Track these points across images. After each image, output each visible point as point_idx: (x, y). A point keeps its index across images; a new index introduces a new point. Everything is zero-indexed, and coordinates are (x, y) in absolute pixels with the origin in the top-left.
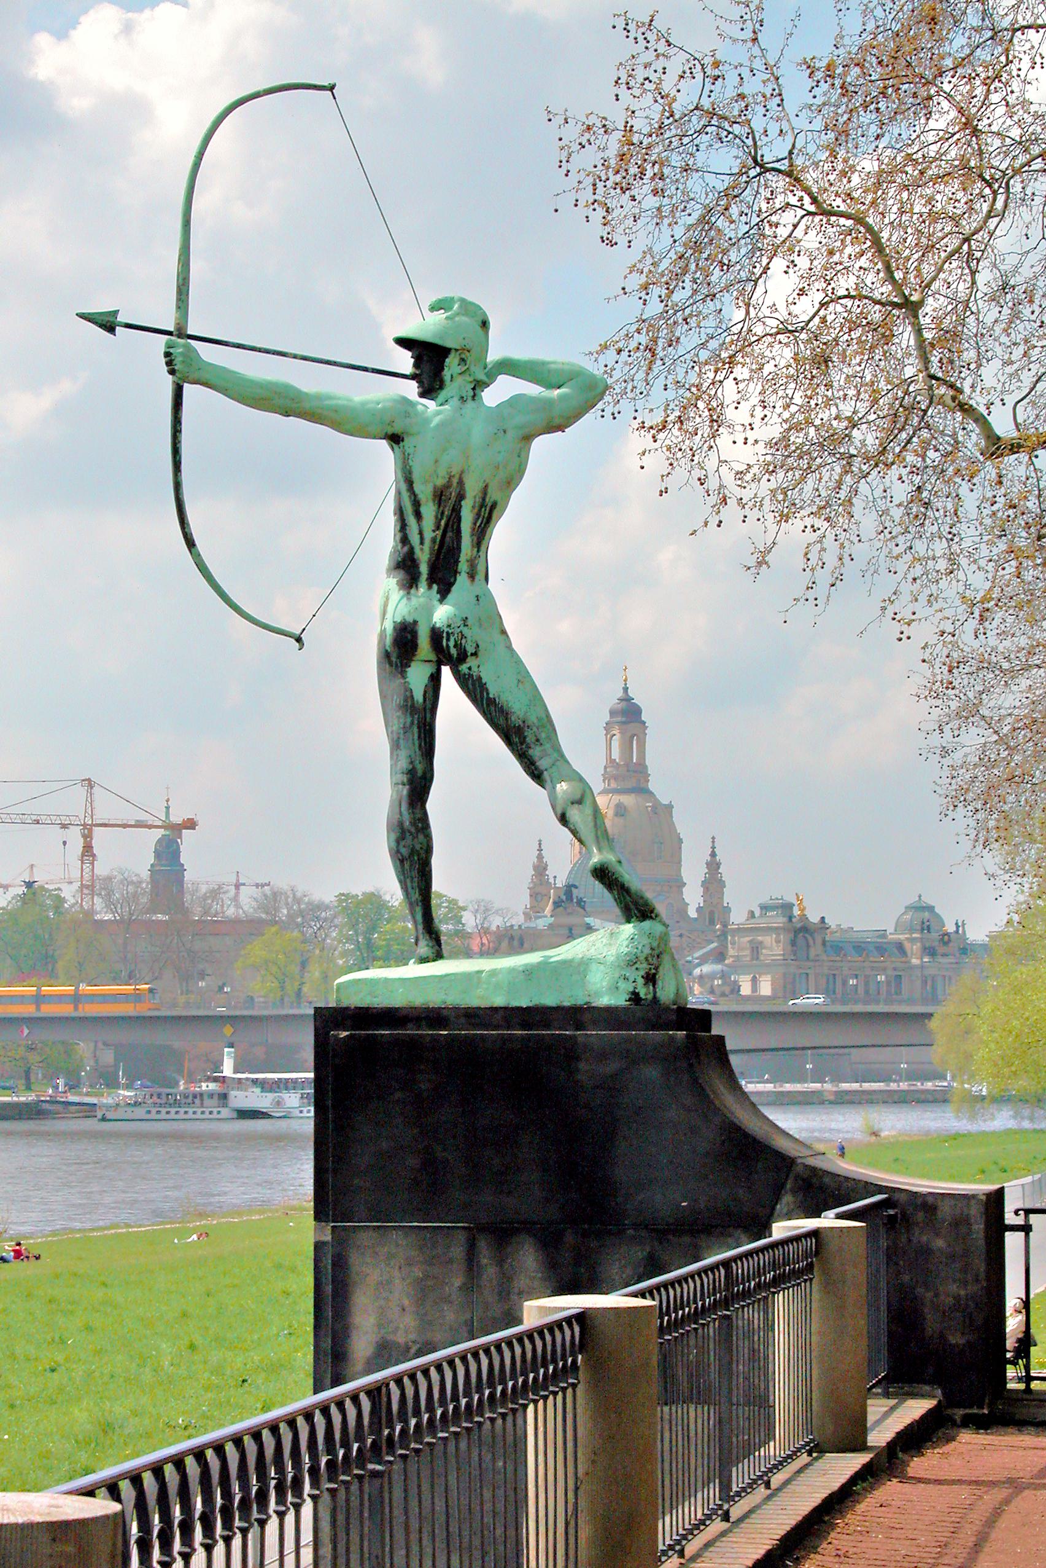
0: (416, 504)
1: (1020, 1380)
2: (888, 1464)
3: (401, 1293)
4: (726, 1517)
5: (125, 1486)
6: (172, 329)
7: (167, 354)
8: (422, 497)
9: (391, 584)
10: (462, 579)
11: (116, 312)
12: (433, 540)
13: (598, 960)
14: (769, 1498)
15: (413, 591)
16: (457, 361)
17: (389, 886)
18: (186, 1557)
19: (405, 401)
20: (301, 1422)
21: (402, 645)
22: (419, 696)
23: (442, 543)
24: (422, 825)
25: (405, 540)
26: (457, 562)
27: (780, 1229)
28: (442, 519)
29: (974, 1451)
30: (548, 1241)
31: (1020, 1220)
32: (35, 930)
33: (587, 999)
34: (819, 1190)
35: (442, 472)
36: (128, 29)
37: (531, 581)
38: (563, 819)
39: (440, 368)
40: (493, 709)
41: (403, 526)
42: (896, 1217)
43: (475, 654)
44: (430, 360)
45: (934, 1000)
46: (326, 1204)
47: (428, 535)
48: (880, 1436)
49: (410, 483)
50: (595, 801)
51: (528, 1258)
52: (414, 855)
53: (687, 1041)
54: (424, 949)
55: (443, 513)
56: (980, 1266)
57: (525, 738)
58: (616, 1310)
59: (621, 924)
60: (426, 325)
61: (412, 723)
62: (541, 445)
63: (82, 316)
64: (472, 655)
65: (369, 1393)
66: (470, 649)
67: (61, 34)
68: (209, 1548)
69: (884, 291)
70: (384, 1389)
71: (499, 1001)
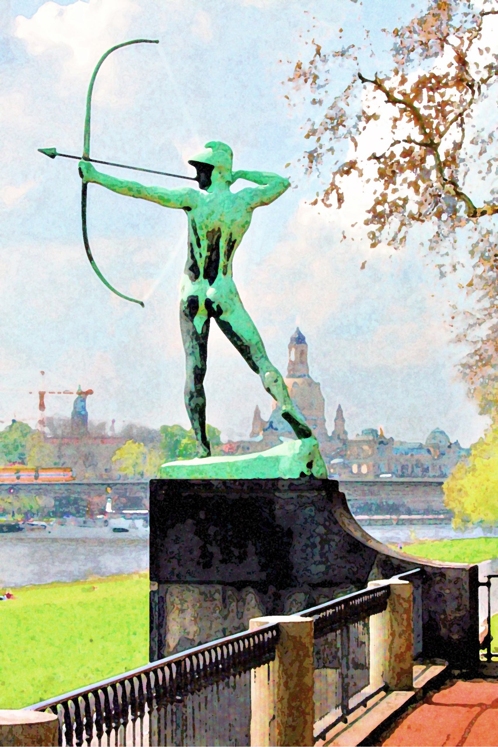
0: (198, 240)
1: (485, 656)
2: (423, 696)
3: (189, 616)
4: (346, 721)
5: (59, 707)
6: (81, 156)
7: (80, 169)
9: (185, 278)
10: (220, 275)
13: (285, 459)
14: (366, 712)
17: (184, 421)
18: (89, 741)
19: (193, 191)
20: (143, 676)
21: (192, 305)
22: (199, 331)
23: (211, 259)
24: (200, 392)
25: (193, 257)
27: (371, 586)
29: (463, 690)
30: (261, 588)
31: (485, 580)
32: (15, 443)
34: (391, 566)
36: (61, 14)
37: (251, 280)
38: (268, 390)
41: (192, 251)
42: (426, 577)
44: (204, 172)
45: (444, 476)
46: (155, 575)
48: (419, 683)
49: (196, 233)
50: (283, 381)
51: (251, 597)
52: (198, 412)
53: (327, 493)
54: (202, 450)
56: (466, 602)
58: (294, 623)
59: (296, 440)
60: (203, 155)
62: (258, 211)
65: (175, 663)
67: (29, 17)
68: (99, 736)
69: (420, 138)
70: (183, 663)
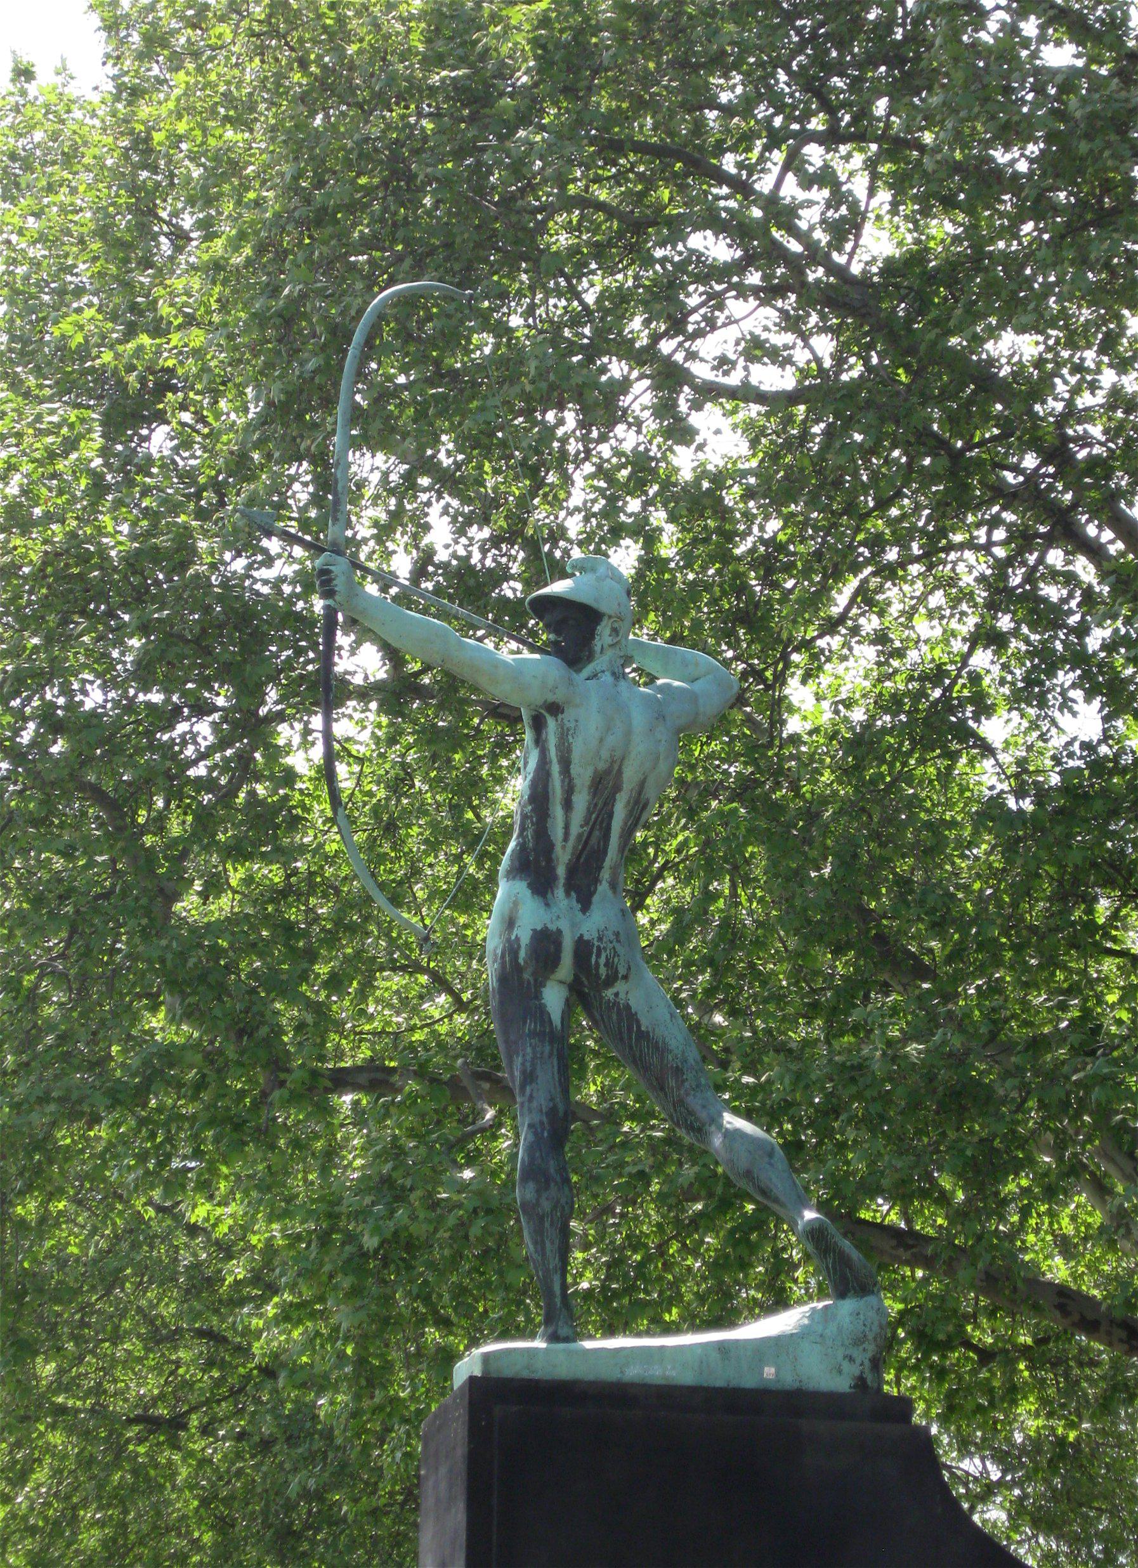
8: (577, 782)
12: (580, 836)
16: (607, 631)
26: (600, 868)
35: (605, 754)
39: (588, 635)
43: (625, 977)
47: (575, 830)
66: (622, 971)
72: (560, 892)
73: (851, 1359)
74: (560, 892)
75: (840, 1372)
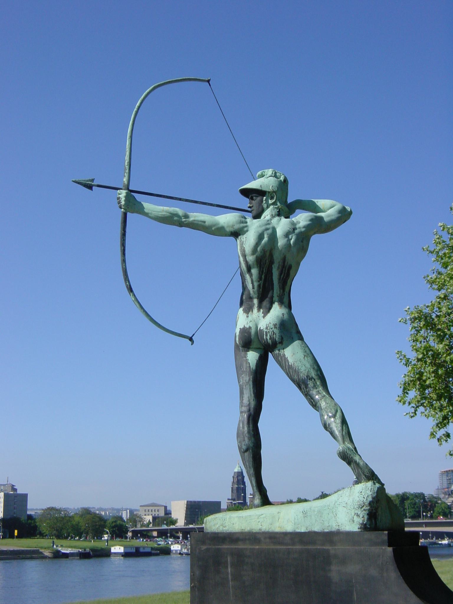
11: (93, 180)
12: (259, 286)
15: (250, 313)
28: (262, 274)
33: (337, 528)
40: (291, 371)
55: (263, 271)
57: (308, 385)
61: (249, 380)
63: (74, 181)
64: (280, 343)
71: (289, 528)
72: (255, 310)
73: (358, 516)
74: (255, 310)
75: (353, 521)
